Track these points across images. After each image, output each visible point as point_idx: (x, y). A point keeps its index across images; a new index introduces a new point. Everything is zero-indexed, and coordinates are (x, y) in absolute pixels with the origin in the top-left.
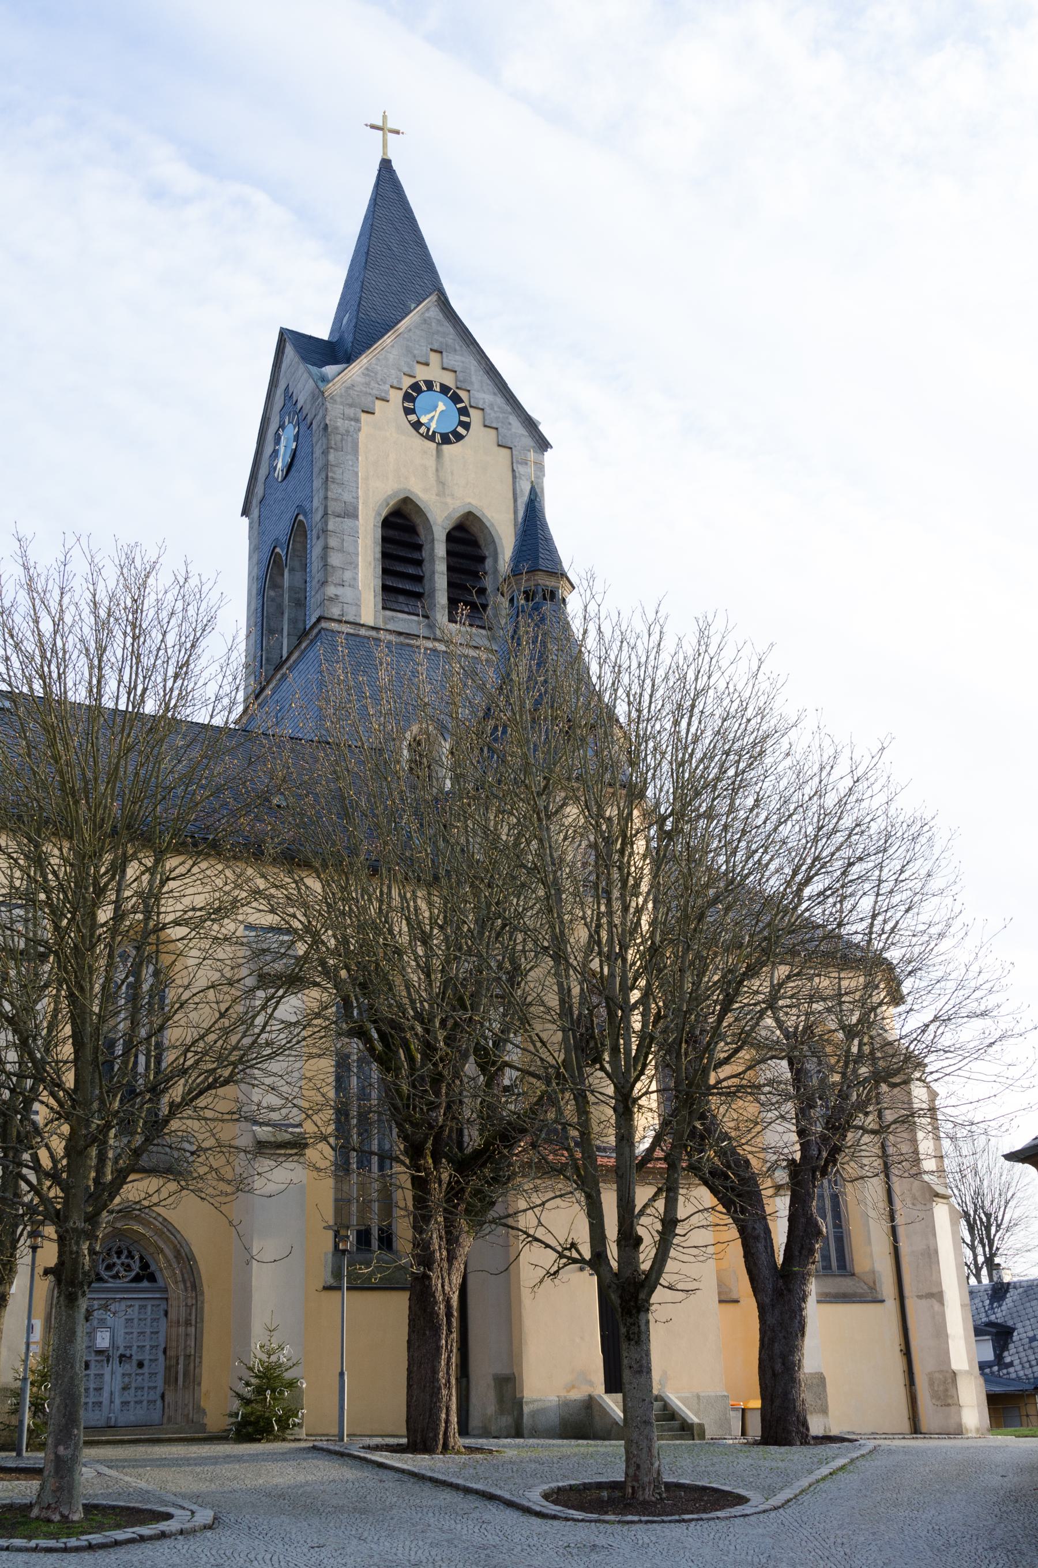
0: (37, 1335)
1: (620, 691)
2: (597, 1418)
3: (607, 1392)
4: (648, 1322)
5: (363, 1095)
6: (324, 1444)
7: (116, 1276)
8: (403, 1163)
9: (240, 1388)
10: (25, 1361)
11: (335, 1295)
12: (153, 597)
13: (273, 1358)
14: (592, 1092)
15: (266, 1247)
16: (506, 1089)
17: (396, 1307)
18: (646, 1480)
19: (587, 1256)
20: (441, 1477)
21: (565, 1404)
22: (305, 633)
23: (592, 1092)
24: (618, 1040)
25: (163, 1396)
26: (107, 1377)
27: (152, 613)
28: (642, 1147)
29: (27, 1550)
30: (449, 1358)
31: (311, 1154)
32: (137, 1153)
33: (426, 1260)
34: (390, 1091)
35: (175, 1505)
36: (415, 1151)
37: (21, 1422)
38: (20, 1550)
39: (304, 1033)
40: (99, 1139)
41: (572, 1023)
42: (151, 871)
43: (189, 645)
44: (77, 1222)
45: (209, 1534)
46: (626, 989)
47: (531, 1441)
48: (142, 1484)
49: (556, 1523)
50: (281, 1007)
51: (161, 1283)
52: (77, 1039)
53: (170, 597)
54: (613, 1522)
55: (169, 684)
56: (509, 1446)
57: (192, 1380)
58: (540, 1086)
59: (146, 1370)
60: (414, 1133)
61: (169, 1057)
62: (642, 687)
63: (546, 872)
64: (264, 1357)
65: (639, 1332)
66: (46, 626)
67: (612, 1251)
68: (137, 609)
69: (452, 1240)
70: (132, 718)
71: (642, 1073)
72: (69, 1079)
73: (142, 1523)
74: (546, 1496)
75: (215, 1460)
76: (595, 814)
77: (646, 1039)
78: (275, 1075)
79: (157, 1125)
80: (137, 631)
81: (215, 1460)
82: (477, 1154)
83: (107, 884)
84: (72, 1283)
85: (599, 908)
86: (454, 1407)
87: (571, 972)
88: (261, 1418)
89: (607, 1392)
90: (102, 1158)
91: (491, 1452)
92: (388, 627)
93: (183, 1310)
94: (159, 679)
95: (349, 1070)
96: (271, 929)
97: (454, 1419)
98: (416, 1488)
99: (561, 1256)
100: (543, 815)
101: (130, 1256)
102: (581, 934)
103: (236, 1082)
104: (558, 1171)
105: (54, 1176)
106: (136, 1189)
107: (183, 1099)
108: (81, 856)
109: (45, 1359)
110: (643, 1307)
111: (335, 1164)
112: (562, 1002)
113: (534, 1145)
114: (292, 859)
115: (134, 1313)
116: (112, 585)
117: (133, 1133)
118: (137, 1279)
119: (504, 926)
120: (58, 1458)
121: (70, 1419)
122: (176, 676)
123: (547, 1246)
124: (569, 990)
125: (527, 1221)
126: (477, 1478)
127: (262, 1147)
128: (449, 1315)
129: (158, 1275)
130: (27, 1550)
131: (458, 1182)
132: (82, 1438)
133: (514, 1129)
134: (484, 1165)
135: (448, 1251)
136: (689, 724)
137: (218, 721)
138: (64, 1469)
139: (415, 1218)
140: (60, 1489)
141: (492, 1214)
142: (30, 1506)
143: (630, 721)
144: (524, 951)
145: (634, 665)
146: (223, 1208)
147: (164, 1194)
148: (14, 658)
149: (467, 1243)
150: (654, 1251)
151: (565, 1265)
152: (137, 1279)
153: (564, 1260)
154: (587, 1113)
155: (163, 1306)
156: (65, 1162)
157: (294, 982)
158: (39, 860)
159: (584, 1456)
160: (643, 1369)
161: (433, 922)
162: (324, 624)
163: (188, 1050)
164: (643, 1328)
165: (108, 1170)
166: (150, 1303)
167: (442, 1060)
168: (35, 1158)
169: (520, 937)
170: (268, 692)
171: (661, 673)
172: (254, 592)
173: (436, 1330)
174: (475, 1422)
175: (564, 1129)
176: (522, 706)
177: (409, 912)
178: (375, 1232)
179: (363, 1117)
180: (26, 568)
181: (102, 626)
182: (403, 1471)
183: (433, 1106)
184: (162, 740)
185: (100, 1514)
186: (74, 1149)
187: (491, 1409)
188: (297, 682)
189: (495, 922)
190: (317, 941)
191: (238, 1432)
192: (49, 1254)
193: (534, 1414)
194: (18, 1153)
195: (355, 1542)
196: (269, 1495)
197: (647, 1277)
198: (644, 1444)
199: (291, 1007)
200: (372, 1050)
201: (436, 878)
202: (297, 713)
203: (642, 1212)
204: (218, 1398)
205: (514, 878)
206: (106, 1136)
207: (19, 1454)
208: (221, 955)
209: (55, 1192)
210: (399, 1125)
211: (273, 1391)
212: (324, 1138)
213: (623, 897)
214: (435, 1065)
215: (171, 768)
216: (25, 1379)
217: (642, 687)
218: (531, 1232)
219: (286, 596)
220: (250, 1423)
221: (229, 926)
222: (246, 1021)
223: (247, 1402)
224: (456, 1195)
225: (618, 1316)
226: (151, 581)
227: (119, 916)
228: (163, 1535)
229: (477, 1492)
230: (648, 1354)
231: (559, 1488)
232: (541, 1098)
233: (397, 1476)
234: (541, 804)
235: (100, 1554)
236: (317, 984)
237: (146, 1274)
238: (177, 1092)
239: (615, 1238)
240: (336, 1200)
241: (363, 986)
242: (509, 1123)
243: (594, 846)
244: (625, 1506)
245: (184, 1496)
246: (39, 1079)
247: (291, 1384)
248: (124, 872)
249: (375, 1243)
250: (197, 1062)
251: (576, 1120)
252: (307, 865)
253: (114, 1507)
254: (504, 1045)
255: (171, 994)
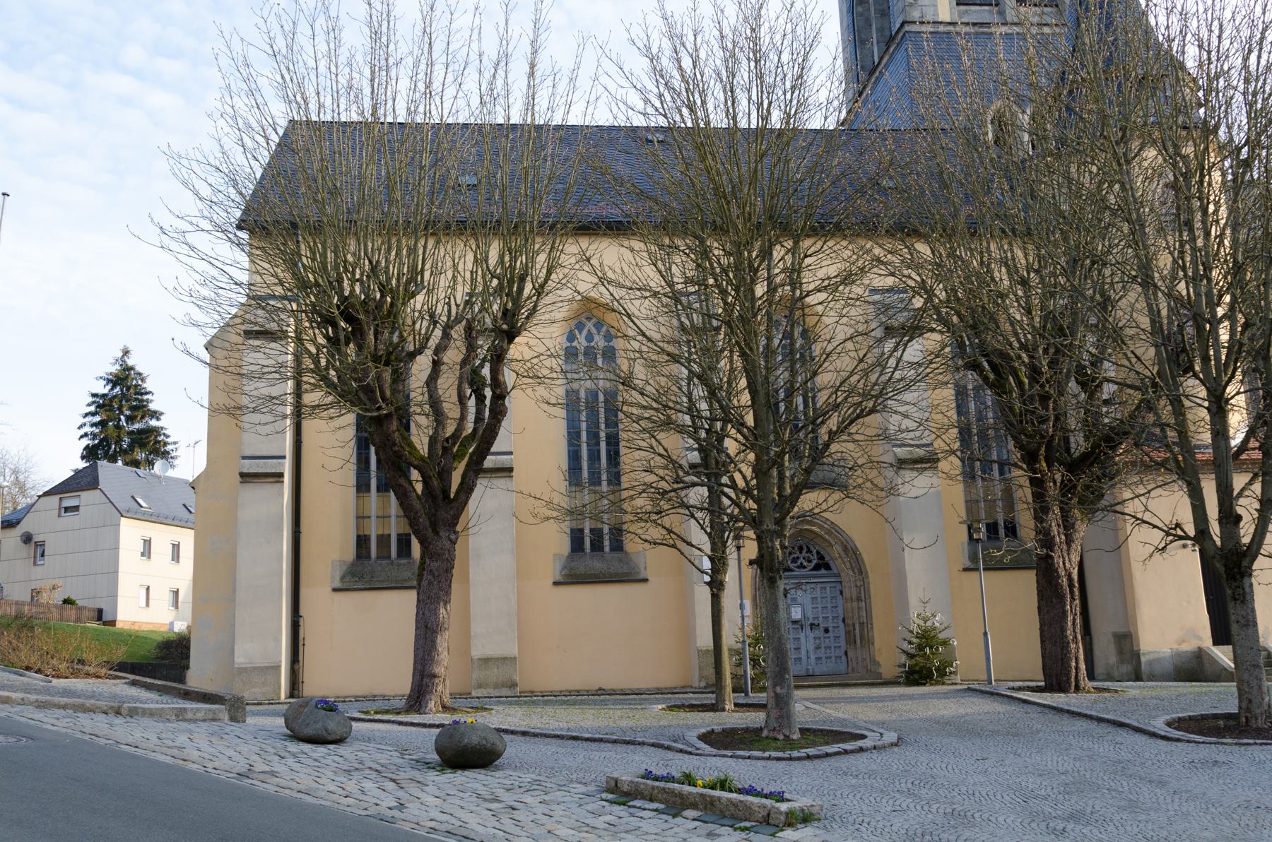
0: (748, 610)
1: (1189, 37)
2: (1207, 665)
3: (1216, 643)
4: (1251, 585)
5: (981, 417)
6: (977, 687)
7: (802, 566)
8: (1022, 469)
9: (906, 646)
10: (742, 629)
11: (975, 575)
12: (767, 25)
13: (929, 624)
14: (1187, 397)
15: (915, 538)
16: (1106, 402)
17: (1027, 581)
18: (1258, 711)
19: (1192, 533)
20: (1076, 710)
21: (1179, 654)
22: (892, 38)
23: (1187, 397)
24: (1207, 350)
25: (846, 653)
26: (803, 640)
27: (767, 40)
28: (1236, 440)
29: (763, 758)
30: (1074, 620)
31: (942, 465)
32: (808, 471)
33: (1047, 542)
34: (1005, 410)
35: (866, 729)
36: (1030, 458)
37: (745, 671)
38: (758, 758)
39: (928, 370)
40: (777, 462)
41: (1163, 339)
42: (793, 251)
43: (800, 60)
44: (769, 525)
45: (896, 749)
46: (1213, 305)
47: (1150, 683)
48: (841, 715)
49: (1179, 744)
50: (908, 350)
51: (835, 571)
52: (752, 387)
53: (781, 21)
54: (1231, 744)
55: (788, 96)
56: (1132, 687)
57: (867, 641)
58: (1138, 395)
59: (831, 634)
60: (1029, 443)
61: (822, 398)
62: (1211, 31)
63: (1129, 210)
64: (921, 623)
65: (1244, 593)
66: (687, 63)
67: (1215, 528)
68: (755, 39)
69: (1068, 526)
70: (760, 133)
71: (1233, 376)
72: (750, 420)
73: (844, 741)
74: (1169, 724)
75: (893, 698)
76: (1172, 154)
77: (1236, 348)
78: (909, 403)
79: (818, 453)
80: (758, 58)
81: (893, 698)
82: (1085, 457)
83: (759, 266)
84: (771, 569)
85: (1181, 236)
86: (1081, 657)
87: (1160, 295)
88: (924, 667)
89: (1216, 643)
90: (781, 477)
91: (1116, 691)
92: (964, 20)
93: (854, 589)
94: (780, 93)
95: (967, 395)
96: (891, 290)
97: (1083, 666)
98: (1057, 717)
99: (1168, 534)
100: (1122, 161)
101: (809, 551)
102: (1164, 261)
103: (878, 411)
104: (1162, 464)
105: (747, 493)
106: (808, 501)
107: (838, 427)
108: (738, 245)
109: (756, 628)
110: (1248, 573)
111: (963, 473)
112: (1153, 322)
113: (1137, 445)
114: (904, 230)
115: (818, 594)
116: (733, 21)
117: (801, 458)
118: (817, 568)
119: (1093, 263)
120: (777, 696)
121: (782, 669)
122: (793, 88)
123: (1155, 527)
124: (1159, 311)
125: (1134, 507)
126: (1107, 710)
127: (901, 464)
128: (1071, 586)
129: (831, 563)
130: (763, 758)
131: (1070, 480)
132: (793, 684)
133: (1117, 434)
134: (1091, 465)
135: (1066, 536)
136: (1259, 57)
137: (831, 125)
138: (782, 703)
139: (1035, 510)
140: (781, 717)
141: (1104, 503)
142: (761, 729)
143: (1200, 66)
144: (1112, 284)
145: (1201, 10)
146: (879, 509)
147: (831, 502)
148: (666, 94)
149: (1082, 529)
150: (1253, 527)
151: (1172, 542)
152: (817, 568)
153: (1171, 538)
154: (1184, 415)
155: (839, 587)
156: (754, 482)
157: (913, 330)
158: (705, 253)
159: (1199, 694)
160: (1250, 622)
161: (1029, 269)
162: (907, 28)
163: (837, 390)
164: (1247, 589)
165: (787, 486)
166: (828, 586)
167: (1048, 382)
168: (732, 479)
169: (1107, 272)
170: (868, 91)
171: (1228, 14)
172: (845, 10)
173: (1061, 598)
174: (1099, 669)
175: (1163, 430)
176: (1096, 64)
177: (1006, 262)
178: (1001, 523)
179: (983, 435)
180: (665, 18)
181: (731, 58)
182: (1044, 706)
183: (1044, 420)
184: (788, 144)
185: (813, 735)
186: (759, 471)
187: (1113, 659)
188: (892, 77)
189: (1083, 261)
190: (930, 294)
191: (907, 678)
192: (751, 549)
193: (1150, 663)
194: (718, 476)
195: (1012, 756)
196: (938, 722)
197: (1248, 548)
198: (1254, 683)
199: (914, 351)
200: (985, 379)
201: (1029, 234)
202: (893, 111)
203: (1240, 494)
204: (889, 651)
205: (1100, 220)
206: (783, 459)
207: (747, 694)
208: (853, 312)
209: (751, 504)
210: (1015, 438)
211: (931, 648)
212: (954, 452)
213: (1204, 222)
214: (1042, 386)
215: (797, 166)
216: (744, 642)
217: (1211, 31)
218: (1139, 516)
219: (872, 9)
220: (916, 672)
221: (858, 290)
222: (881, 364)
223: (911, 656)
224: (1069, 491)
225: (1224, 580)
226: (763, 12)
227: (772, 289)
228: (861, 750)
229: (1108, 721)
230: (1253, 610)
231: (1180, 719)
232: (1138, 407)
233: (1040, 709)
234: (1120, 151)
235: (816, 762)
236: (933, 330)
237: (822, 565)
238: (833, 423)
239: (1216, 516)
240: (966, 501)
241: (974, 327)
242: (1112, 429)
243: (1173, 186)
244: (1241, 732)
245: (872, 723)
246: (726, 421)
247: (945, 643)
248: (771, 254)
249: (1002, 532)
250: (846, 398)
251: (1173, 421)
252: (916, 233)
253: (821, 731)
254: (1102, 363)
255: (817, 349)
